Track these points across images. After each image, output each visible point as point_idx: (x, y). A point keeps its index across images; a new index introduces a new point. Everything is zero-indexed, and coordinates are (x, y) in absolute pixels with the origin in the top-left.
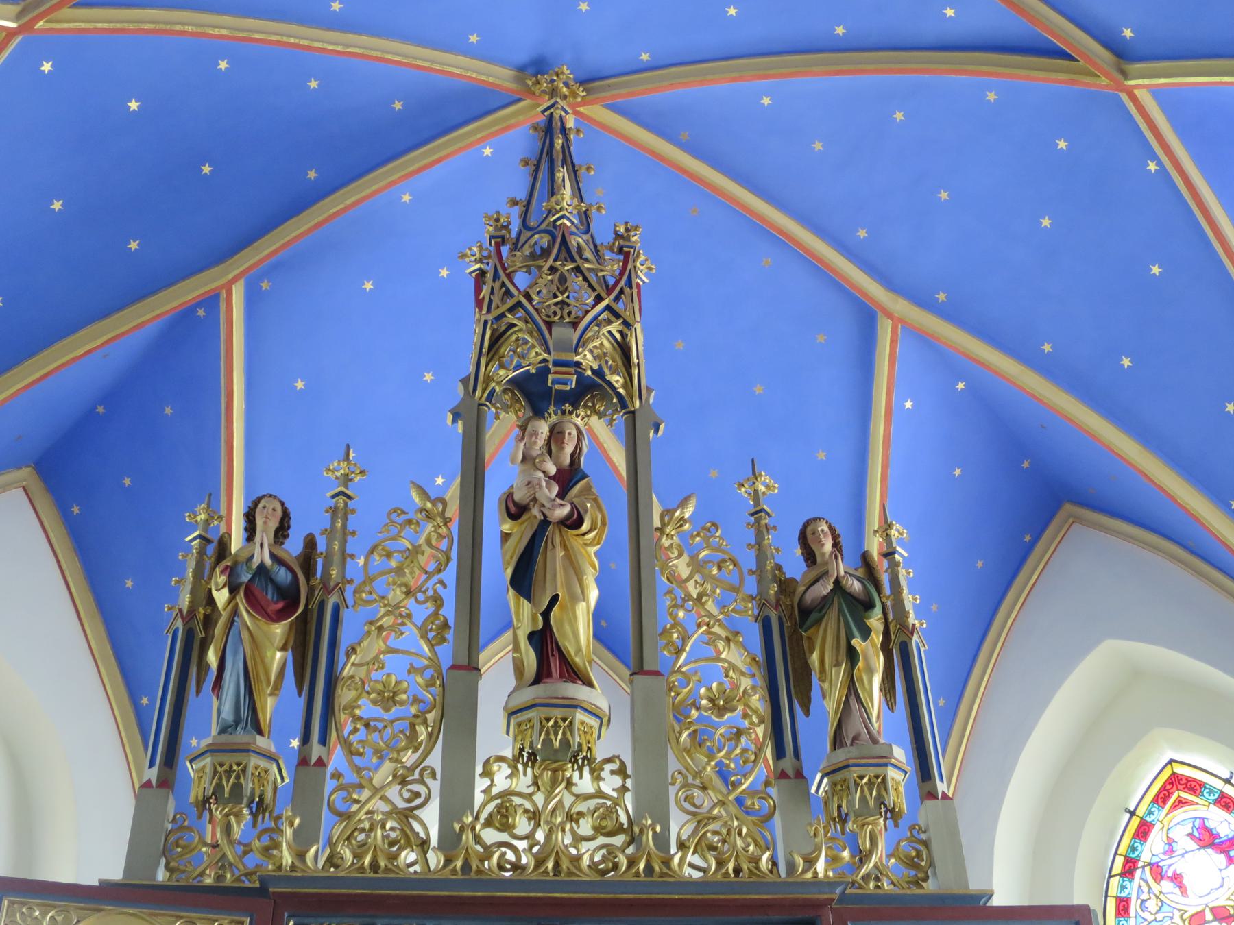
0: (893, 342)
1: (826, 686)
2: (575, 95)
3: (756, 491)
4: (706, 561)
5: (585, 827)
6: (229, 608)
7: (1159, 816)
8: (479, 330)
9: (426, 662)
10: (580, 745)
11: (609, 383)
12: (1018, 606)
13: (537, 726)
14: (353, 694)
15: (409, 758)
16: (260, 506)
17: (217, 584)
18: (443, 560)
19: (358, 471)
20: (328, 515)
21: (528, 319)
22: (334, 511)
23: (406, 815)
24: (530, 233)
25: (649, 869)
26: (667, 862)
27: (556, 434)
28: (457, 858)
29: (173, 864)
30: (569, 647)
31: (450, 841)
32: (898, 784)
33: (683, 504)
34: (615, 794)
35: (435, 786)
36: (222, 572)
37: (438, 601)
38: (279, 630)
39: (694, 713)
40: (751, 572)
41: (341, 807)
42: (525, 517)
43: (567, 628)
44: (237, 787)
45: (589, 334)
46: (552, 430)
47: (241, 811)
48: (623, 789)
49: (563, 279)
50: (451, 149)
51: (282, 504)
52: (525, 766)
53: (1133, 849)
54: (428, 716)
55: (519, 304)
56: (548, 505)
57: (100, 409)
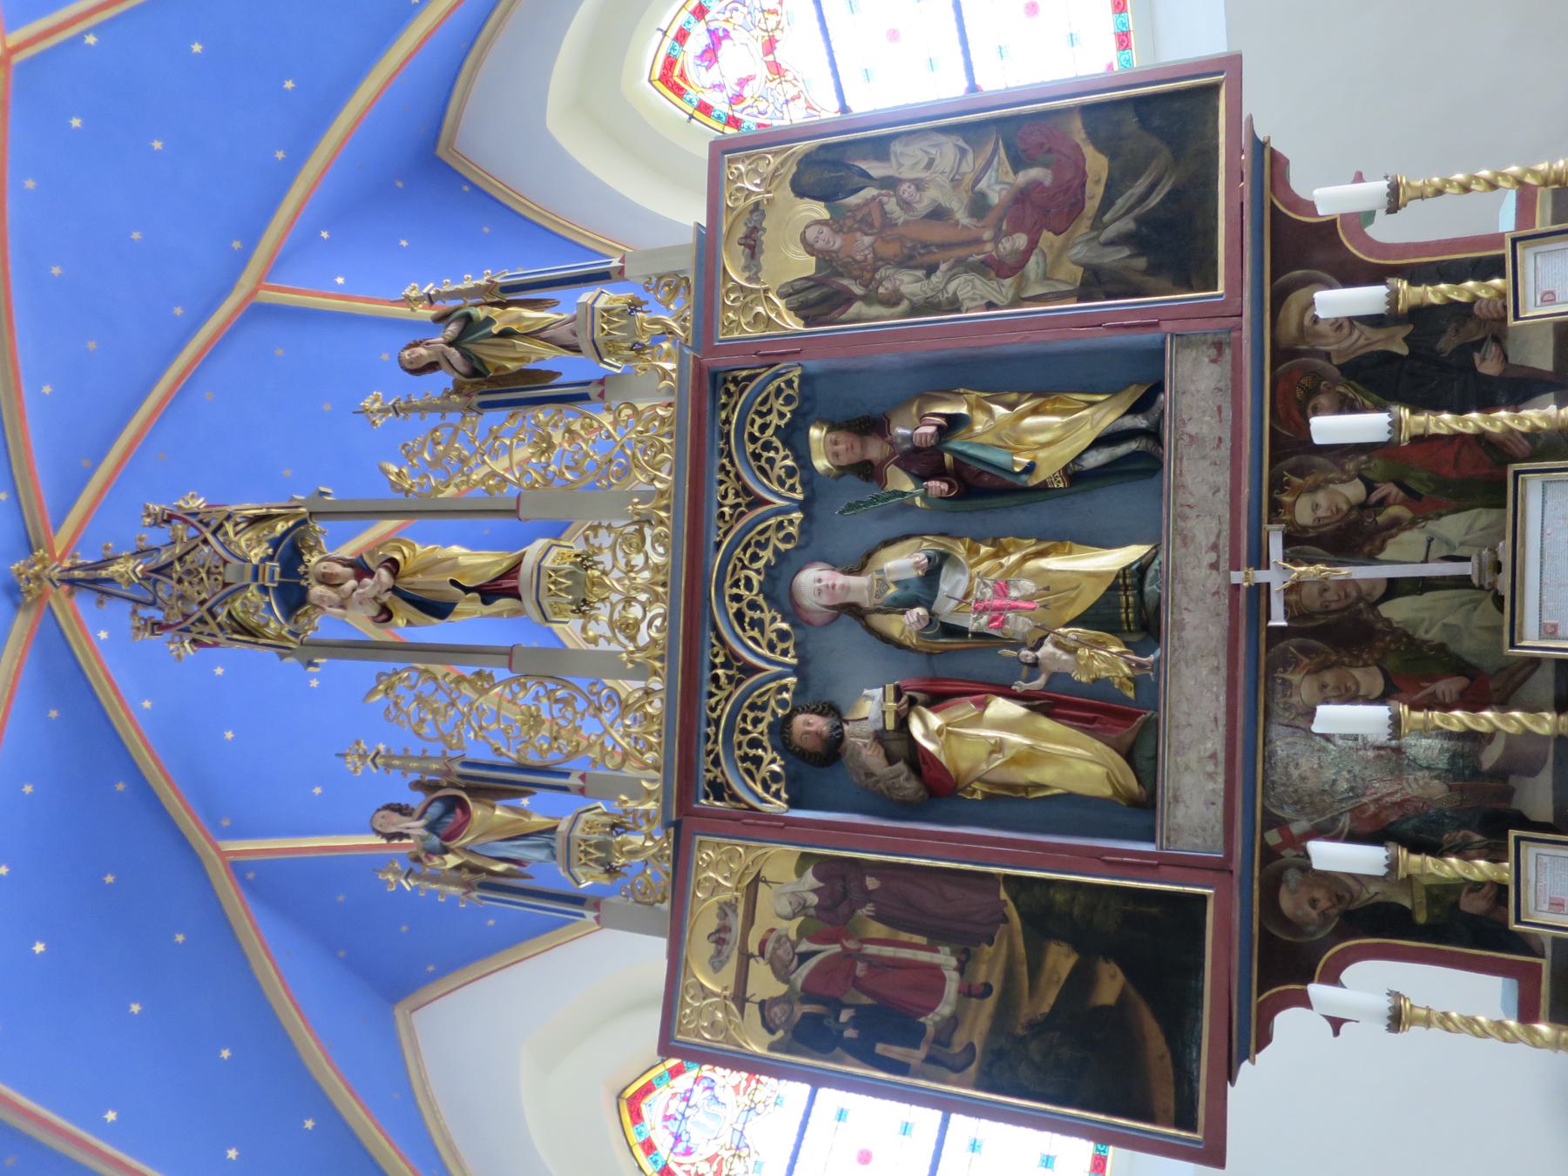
0: (279, 290)
1: (533, 357)
2: (42, 559)
3: (379, 411)
4: (432, 454)
5: (638, 560)
6: (461, 854)
7: (692, 94)
8: (238, 645)
9: (507, 690)
10: (572, 563)
11: (285, 534)
12: (523, 200)
13: (555, 599)
14: (530, 749)
16: (379, 829)
17: (442, 865)
18: (425, 675)
19: (356, 747)
20: (392, 771)
21: (222, 601)
22: (388, 766)
23: (625, 707)
24: (158, 600)
25: (666, 508)
26: (662, 493)
27: (327, 580)
28: (653, 666)
29: (659, 897)
30: (494, 572)
31: (642, 671)
32: (610, 299)
33: (386, 473)
34: (613, 535)
36: (430, 860)
37: (460, 679)
38: (478, 811)
39: (552, 468)
40: (443, 416)
41: (618, 759)
42: (391, 607)
43: (479, 572)
44: (598, 846)
45: (238, 552)
46: (321, 582)
47: (618, 842)
48: (609, 527)
49: (189, 572)
50: (96, 666)
51: (379, 810)
52: (592, 608)
54: (549, 688)
55: (210, 610)
56: (378, 588)
57: (342, 954)
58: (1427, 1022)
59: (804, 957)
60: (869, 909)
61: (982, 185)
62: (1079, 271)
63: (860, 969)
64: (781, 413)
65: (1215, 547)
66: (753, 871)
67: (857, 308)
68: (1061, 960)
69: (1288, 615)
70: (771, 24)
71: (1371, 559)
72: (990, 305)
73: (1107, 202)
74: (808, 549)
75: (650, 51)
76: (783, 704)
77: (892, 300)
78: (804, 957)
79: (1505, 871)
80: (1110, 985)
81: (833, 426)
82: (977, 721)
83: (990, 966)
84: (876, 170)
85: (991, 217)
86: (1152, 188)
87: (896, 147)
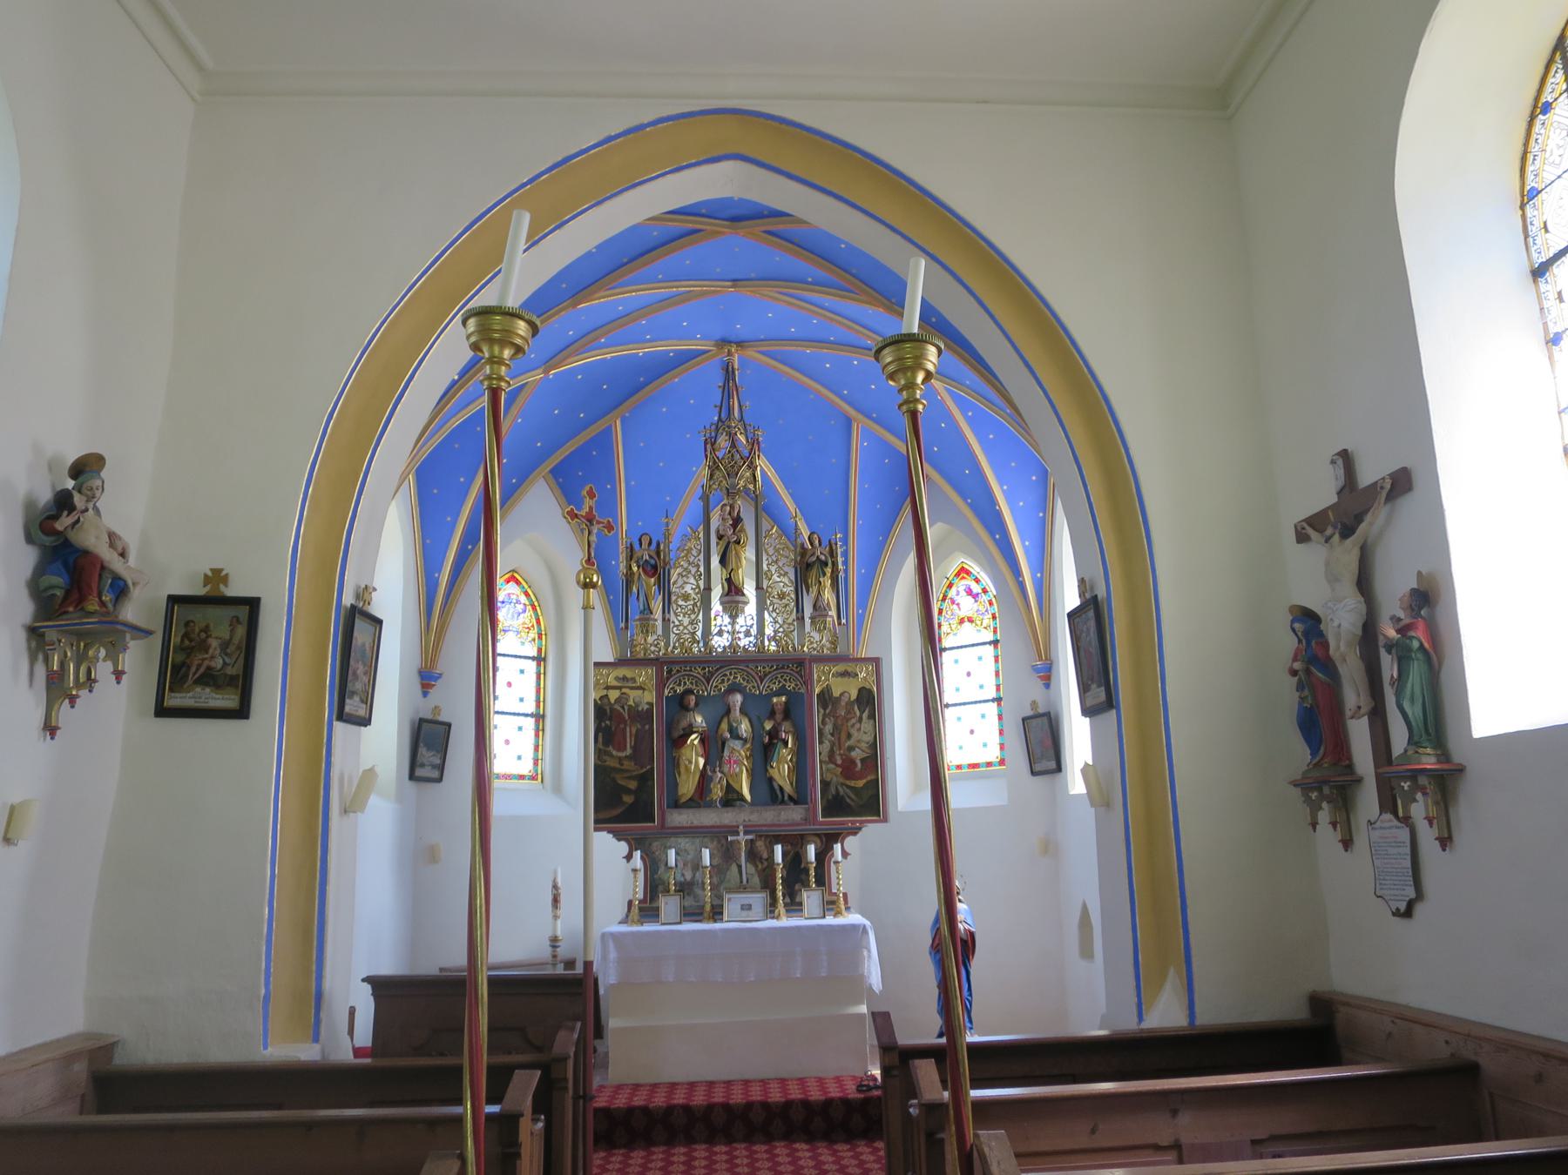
7: (956, 580)
15: (693, 617)
35: (701, 625)
49: (732, 456)
53: (946, 591)
58: (635, 877)
59: (623, 707)
60: (639, 727)
61: (857, 749)
62: (829, 780)
63: (622, 726)
64: (790, 686)
65: (750, 821)
66: (646, 687)
67: (822, 711)
68: (633, 785)
69: (731, 841)
70: (979, 623)
71: (747, 860)
72: (820, 754)
73: (848, 787)
74: (745, 696)
75: (975, 568)
76: (698, 692)
77: (824, 723)
78: (623, 707)
79: (672, 892)
80: (628, 799)
81: (786, 703)
82: (697, 755)
83: (628, 765)
84: (865, 715)
85: (847, 753)
86: (853, 800)
87: (872, 722)
